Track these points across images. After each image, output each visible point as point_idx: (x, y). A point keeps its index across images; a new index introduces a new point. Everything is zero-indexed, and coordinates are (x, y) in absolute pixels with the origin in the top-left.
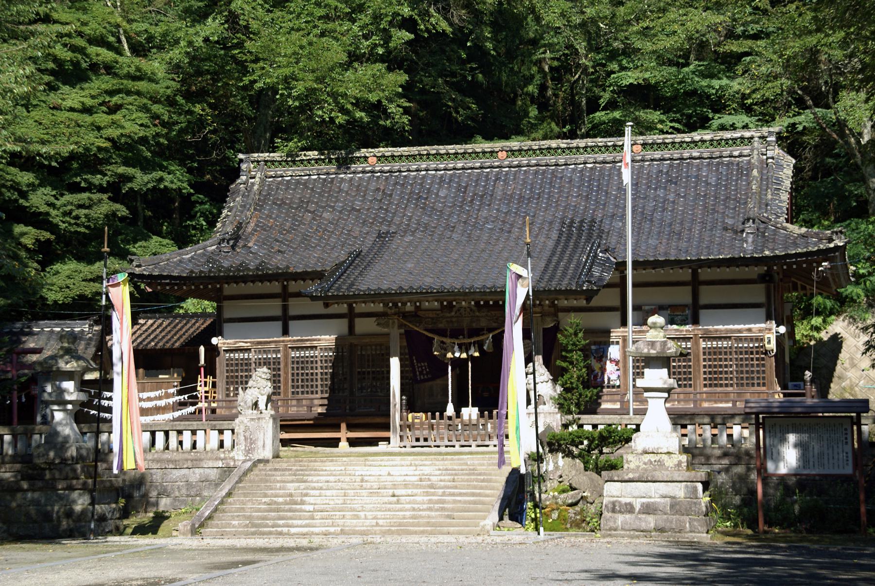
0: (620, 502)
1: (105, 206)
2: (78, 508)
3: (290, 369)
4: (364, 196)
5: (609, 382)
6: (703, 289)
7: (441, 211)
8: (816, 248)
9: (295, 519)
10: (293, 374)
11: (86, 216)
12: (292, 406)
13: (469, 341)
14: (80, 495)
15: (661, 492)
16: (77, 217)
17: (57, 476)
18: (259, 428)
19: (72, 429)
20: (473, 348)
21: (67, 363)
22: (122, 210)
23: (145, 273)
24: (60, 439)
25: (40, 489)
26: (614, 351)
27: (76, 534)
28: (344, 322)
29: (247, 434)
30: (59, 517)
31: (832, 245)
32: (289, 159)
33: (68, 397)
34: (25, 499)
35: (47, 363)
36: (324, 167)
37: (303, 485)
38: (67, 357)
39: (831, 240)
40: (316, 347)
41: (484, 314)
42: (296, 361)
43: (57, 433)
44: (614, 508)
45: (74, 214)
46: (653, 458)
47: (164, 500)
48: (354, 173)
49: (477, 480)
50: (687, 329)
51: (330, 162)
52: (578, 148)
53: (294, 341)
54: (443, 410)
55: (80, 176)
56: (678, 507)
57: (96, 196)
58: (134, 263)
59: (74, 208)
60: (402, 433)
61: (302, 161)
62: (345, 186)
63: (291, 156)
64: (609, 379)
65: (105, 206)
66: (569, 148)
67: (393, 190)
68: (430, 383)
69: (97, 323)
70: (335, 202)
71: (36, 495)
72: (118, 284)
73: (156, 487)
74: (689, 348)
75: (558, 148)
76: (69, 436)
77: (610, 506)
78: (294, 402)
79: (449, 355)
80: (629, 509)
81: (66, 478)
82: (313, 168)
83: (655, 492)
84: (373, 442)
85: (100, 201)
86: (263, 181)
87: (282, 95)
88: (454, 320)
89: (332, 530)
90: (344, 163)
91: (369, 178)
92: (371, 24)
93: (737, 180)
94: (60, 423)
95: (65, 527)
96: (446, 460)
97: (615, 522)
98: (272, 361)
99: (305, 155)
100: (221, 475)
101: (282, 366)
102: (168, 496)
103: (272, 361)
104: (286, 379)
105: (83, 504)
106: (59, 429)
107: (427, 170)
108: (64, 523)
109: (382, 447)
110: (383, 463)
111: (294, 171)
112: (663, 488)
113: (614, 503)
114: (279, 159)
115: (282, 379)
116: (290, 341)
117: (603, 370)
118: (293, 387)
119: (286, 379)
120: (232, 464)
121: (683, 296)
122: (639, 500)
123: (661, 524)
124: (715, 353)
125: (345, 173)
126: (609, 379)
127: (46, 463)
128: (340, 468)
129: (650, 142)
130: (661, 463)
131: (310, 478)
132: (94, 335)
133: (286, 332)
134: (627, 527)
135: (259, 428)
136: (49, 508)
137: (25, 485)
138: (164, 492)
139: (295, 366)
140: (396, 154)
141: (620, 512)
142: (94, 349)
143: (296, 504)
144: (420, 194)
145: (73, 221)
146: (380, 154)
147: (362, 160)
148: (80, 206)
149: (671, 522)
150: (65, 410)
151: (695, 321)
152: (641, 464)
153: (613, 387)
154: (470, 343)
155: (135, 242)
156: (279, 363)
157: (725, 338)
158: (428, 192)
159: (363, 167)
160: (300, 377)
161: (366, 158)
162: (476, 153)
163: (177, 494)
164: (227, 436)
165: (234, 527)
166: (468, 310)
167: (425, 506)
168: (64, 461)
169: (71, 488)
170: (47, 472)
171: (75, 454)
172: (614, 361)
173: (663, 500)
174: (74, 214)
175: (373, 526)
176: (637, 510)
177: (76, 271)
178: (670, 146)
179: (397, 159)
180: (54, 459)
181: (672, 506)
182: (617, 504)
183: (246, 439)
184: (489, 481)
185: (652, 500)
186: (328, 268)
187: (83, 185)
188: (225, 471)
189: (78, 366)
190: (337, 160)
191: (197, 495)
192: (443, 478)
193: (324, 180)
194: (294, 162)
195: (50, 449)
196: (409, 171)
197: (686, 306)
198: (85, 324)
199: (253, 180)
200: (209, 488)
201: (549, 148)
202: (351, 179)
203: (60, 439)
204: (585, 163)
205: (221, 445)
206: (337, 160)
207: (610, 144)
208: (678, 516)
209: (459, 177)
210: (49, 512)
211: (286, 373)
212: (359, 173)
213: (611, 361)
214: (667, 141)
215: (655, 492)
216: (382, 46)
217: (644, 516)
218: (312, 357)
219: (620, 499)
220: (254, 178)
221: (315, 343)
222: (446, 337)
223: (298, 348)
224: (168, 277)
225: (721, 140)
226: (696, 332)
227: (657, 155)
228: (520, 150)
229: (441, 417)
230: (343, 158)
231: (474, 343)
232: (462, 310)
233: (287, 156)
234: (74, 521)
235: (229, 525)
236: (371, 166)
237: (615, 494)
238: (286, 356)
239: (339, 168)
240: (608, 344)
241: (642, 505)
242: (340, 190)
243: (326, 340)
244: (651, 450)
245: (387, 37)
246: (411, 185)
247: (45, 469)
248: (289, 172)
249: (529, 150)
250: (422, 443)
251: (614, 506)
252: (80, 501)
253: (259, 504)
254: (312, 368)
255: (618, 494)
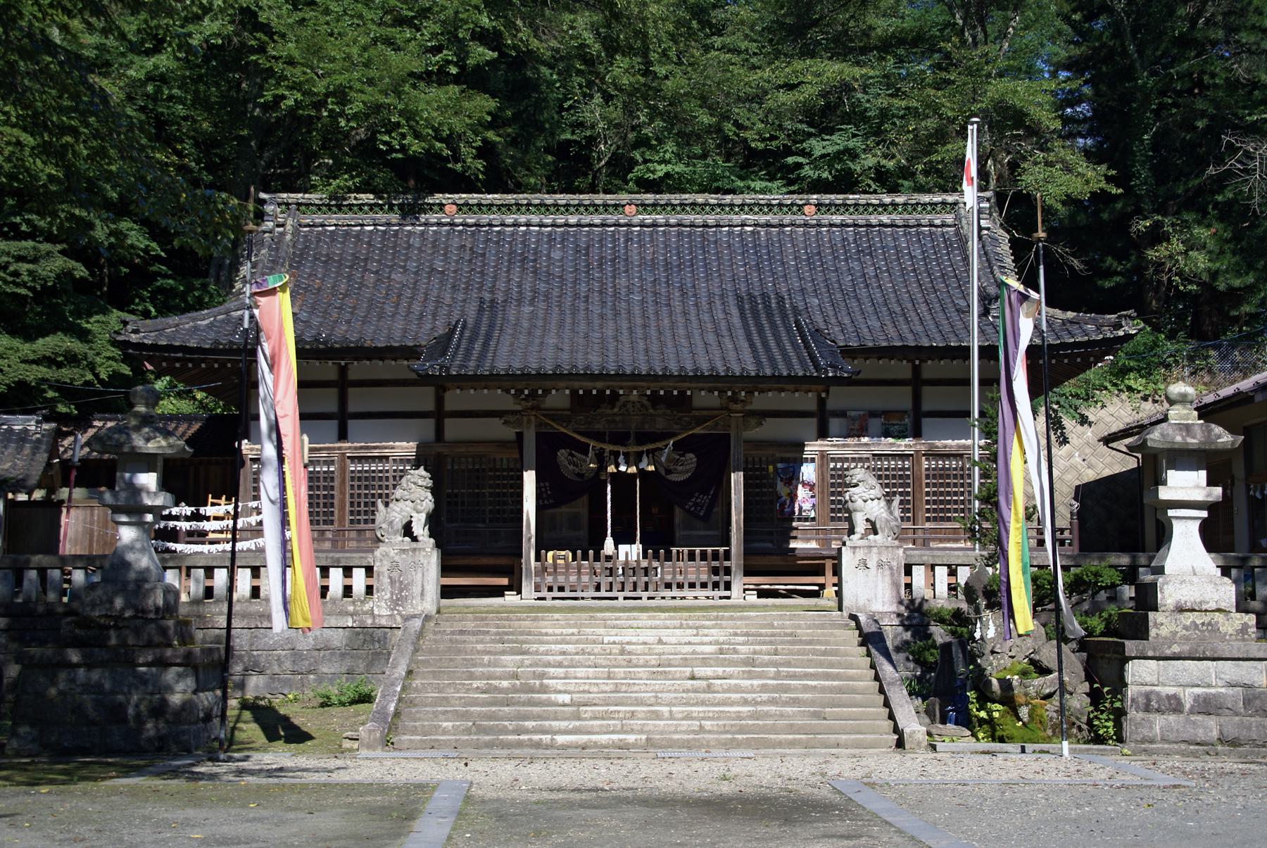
0: (1158, 694)
1: (55, 264)
2: (176, 699)
3: (348, 488)
4: (445, 254)
5: (800, 513)
6: (927, 390)
7: (560, 277)
8: (1101, 337)
9: (547, 719)
10: (352, 496)
11: (30, 273)
12: (349, 540)
13: (640, 449)
14: (180, 676)
15: (1227, 677)
16: (16, 274)
17: (131, 641)
18: (416, 565)
19: (151, 558)
20: (645, 460)
21: (148, 440)
22: (81, 271)
23: (146, 341)
24: (132, 575)
25: (102, 664)
26: (808, 472)
27: (174, 748)
28: (428, 426)
29: (395, 574)
30: (138, 715)
31: (1121, 333)
32: (333, 202)
33: (148, 502)
34: (73, 681)
35: (110, 438)
36: (381, 217)
37: (528, 659)
38: (147, 430)
39: (1118, 326)
40: (387, 458)
41: (660, 412)
42: (358, 478)
43: (127, 565)
44: (1149, 704)
45: (11, 268)
46: (1198, 618)
47: (254, 678)
48: (425, 224)
49: (815, 652)
50: (905, 445)
51: (391, 208)
52: (732, 205)
53: (356, 448)
54: (600, 545)
55: (20, 215)
56: (1258, 702)
57: (46, 247)
58: (129, 328)
59: (11, 260)
60: (538, 579)
61: (350, 206)
62: (416, 242)
63: (336, 199)
64: (801, 508)
65: (55, 264)
66: (719, 205)
67: (485, 249)
68: (551, 511)
69: (47, 419)
70: (405, 261)
71: (95, 675)
72: (273, 292)
73: (241, 657)
74: (908, 469)
75: (705, 205)
76: (147, 570)
77: (1142, 700)
78: (353, 534)
79: (612, 469)
80: (1174, 705)
81: (150, 645)
82: (369, 219)
83: (1216, 677)
84: (498, 592)
85: (48, 254)
86: (296, 233)
87: (331, 111)
88: (618, 419)
89: (631, 738)
90: (411, 211)
91: (448, 233)
92: (442, 34)
93: (948, 254)
94: (131, 548)
95: (152, 733)
96: (722, 618)
97: (1151, 728)
98: (321, 475)
99: (356, 198)
100: (350, 639)
101: (336, 484)
102: (261, 673)
103: (321, 475)
104: (342, 501)
105: (184, 692)
106: (130, 557)
107: (528, 225)
108: (149, 726)
109: (510, 598)
110: (634, 623)
111: (338, 219)
112: (1230, 670)
113: (1148, 696)
114: (317, 202)
115: (336, 502)
116: (350, 448)
117: (793, 497)
118: (352, 513)
119: (342, 501)
120: (369, 622)
121: (901, 399)
122: (1189, 690)
123: (1231, 732)
124: (941, 477)
125: (413, 225)
126: (801, 508)
127: (106, 616)
128: (571, 631)
129: (827, 202)
130: (1212, 627)
131: (534, 647)
132: (43, 435)
133: (343, 436)
134: (1172, 737)
135: (416, 565)
136: (120, 697)
137: (75, 657)
138: (254, 667)
139: (356, 483)
140: (484, 202)
141: (1158, 711)
142: (46, 455)
143: (533, 692)
144: (523, 255)
145: (10, 279)
146: (462, 202)
147: (436, 208)
148: (20, 259)
149: (1249, 728)
150: (140, 524)
151: (917, 434)
152: (1179, 629)
153: (806, 519)
154: (642, 452)
155: (90, 315)
156: (332, 479)
157: (955, 456)
158: (535, 254)
159: (439, 219)
160: (363, 500)
161: (441, 206)
162: (594, 205)
163: (276, 669)
164: (359, 580)
165: (445, 732)
166: (638, 405)
167: (765, 696)
168: (141, 613)
169: (164, 664)
170: (112, 633)
171: (160, 602)
172: (808, 484)
173: (1231, 691)
174: (11, 268)
175: (694, 732)
176: (1188, 706)
177: (11, 348)
178: (851, 210)
179: (484, 209)
180: (123, 609)
181: (1248, 702)
182: (1153, 697)
183: (392, 582)
184: (835, 653)
185: (1213, 691)
186: (424, 343)
187: (24, 228)
188: (358, 634)
189: (170, 446)
190: (401, 206)
191: (310, 672)
192: (758, 648)
193: (384, 232)
194: (339, 207)
195: (116, 593)
196: (503, 225)
197: (905, 412)
198: (29, 420)
199: (281, 229)
200: (330, 660)
201: (694, 204)
202: (423, 233)
203: (132, 575)
204: (743, 225)
205: (348, 591)
206: (401, 206)
207: (774, 202)
208: (1258, 719)
209: (574, 236)
210: (120, 704)
211: (343, 493)
212: (432, 225)
213: (804, 484)
214: (849, 202)
215: (1216, 677)
216: (456, 64)
217: (1200, 718)
218: (381, 471)
219: (1157, 689)
220: (282, 225)
221: (386, 452)
222: (604, 442)
223: (360, 459)
224: (183, 348)
225: (917, 204)
226: (918, 448)
227: (837, 219)
228: (654, 205)
229: (597, 558)
230: (409, 204)
231: (648, 452)
232: (629, 406)
233: (330, 199)
234: (167, 722)
235: (437, 729)
236: (448, 216)
237: (1148, 679)
238: (343, 469)
239: (404, 218)
240: (802, 461)
241: (1196, 698)
242: (410, 246)
243: (402, 448)
244: (1189, 605)
245: (463, 54)
246: (510, 243)
247: (108, 628)
248: (333, 220)
249: (667, 205)
250: (603, 593)
251: (1149, 700)
252: (180, 687)
253: (468, 691)
254: (380, 487)
255: (1154, 679)
